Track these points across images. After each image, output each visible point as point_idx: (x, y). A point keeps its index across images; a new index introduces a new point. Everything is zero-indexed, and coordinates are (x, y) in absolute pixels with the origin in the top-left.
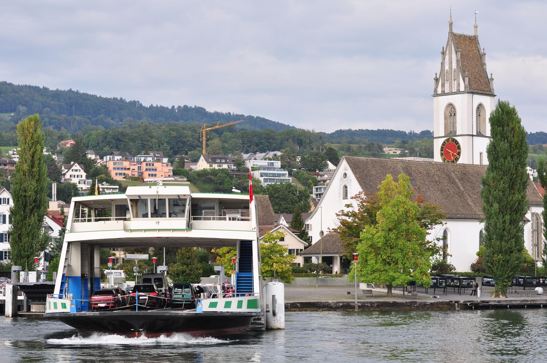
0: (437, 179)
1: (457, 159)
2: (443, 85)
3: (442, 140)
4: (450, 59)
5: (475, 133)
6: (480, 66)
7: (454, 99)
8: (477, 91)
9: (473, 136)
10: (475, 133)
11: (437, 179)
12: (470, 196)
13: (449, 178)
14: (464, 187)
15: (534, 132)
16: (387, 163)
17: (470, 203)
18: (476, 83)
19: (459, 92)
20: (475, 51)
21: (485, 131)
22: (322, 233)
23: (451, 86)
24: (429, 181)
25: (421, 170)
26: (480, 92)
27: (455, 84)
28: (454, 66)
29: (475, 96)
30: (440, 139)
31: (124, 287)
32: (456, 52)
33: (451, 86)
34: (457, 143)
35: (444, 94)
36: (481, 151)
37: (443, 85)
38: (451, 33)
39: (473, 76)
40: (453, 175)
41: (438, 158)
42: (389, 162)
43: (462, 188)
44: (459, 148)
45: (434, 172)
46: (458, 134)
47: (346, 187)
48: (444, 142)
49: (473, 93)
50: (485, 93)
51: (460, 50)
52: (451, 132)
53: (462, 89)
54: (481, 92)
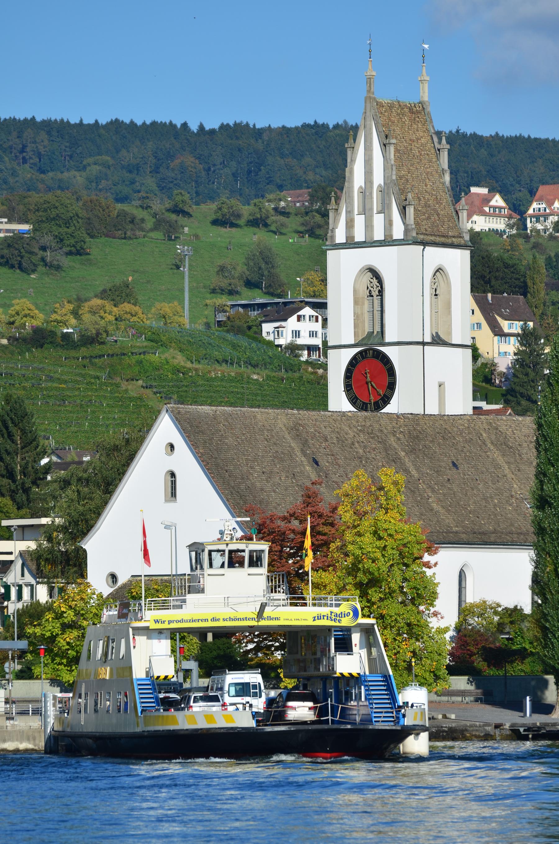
0: (361, 451)
1: (386, 400)
2: (350, 225)
3: (349, 354)
4: (368, 162)
5: (428, 339)
6: (436, 176)
7: (384, 259)
8: (433, 238)
9: (423, 344)
10: (428, 339)
11: (361, 451)
12: (433, 491)
13: (386, 450)
14: (418, 469)
15: (276, 127)
16: (255, 417)
17: (434, 505)
18: (429, 218)
19: (388, 242)
20: (423, 140)
21: (450, 333)
22: (113, 577)
23: (369, 226)
24: (346, 458)
25: (327, 432)
26: (438, 239)
27: (379, 220)
28: (378, 179)
29: (429, 250)
30: (343, 350)
31: (551, 561)
32: (384, 146)
33: (369, 226)
34: (385, 360)
35: (351, 244)
36: (442, 380)
37: (350, 225)
38: (369, 99)
39: (422, 202)
40: (392, 440)
41: (339, 401)
42: (259, 416)
43: (414, 473)
44: (391, 372)
45: (351, 434)
46: (388, 339)
47: (173, 475)
48: (354, 358)
49: (425, 244)
50: (449, 241)
51: (394, 141)
52: (370, 334)
53: (398, 232)
54: (442, 240)
